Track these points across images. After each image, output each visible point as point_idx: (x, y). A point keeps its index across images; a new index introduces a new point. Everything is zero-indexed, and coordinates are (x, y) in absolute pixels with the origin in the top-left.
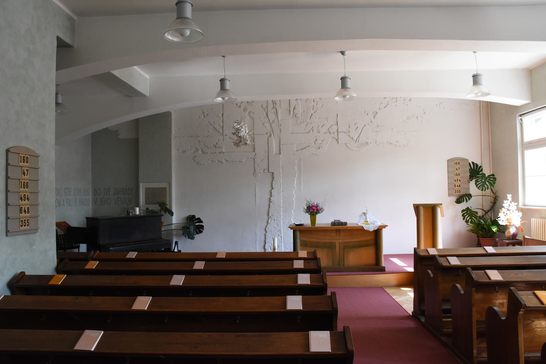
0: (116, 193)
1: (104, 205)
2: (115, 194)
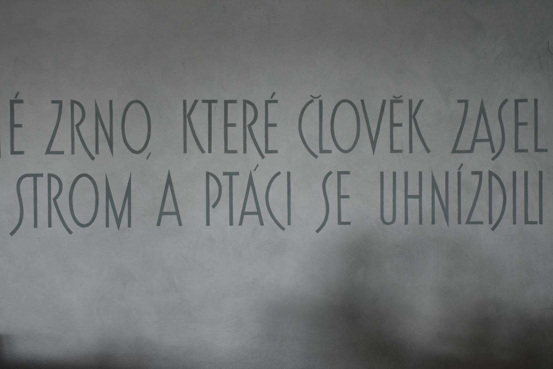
0: (475, 140)
1: (196, 102)
2: (465, 144)
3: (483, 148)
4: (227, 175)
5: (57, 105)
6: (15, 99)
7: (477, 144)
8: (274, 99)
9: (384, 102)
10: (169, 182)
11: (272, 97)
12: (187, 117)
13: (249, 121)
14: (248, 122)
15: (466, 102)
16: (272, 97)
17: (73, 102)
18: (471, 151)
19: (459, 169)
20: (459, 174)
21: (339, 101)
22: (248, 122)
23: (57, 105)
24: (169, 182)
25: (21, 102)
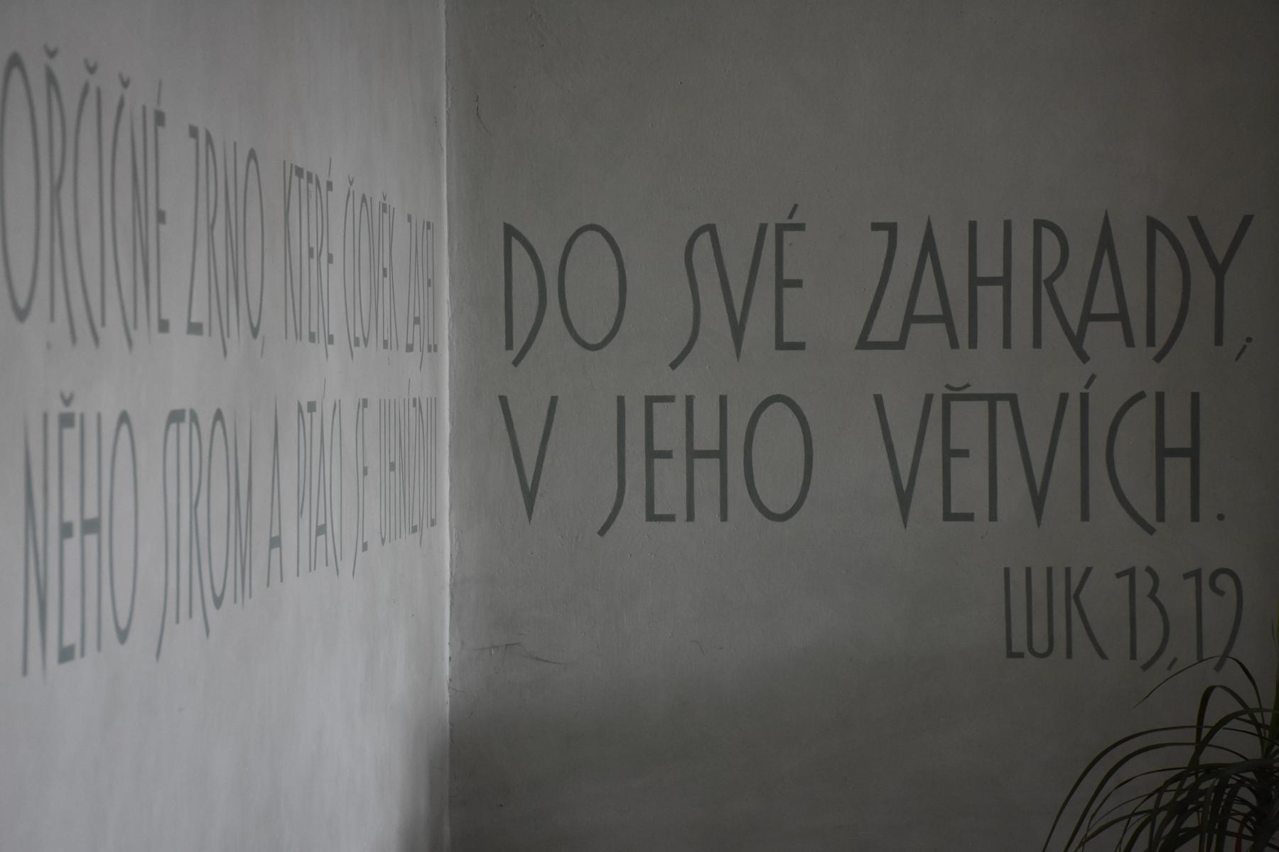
0: (911, 318)
2: (887, 328)
3: (928, 336)
4: (721, 446)
5: (884, 235)
6: (790, 221)
7: (915, 329)
8: (795, 220)
9: (763, 228)
10: (530, 497)
11: (791, 217)
13: (1047, 270)
14: (1046, 272)
15: (891, 228)
16: (791, 217)
17: (1039, 225)
18: (900, 344)
19: (1087, 386)
20: (1084, 398)
21: (578, 227)
22: (1046, 272)
23: (884, 235)
24: (530, 497)
25: (800, 227)
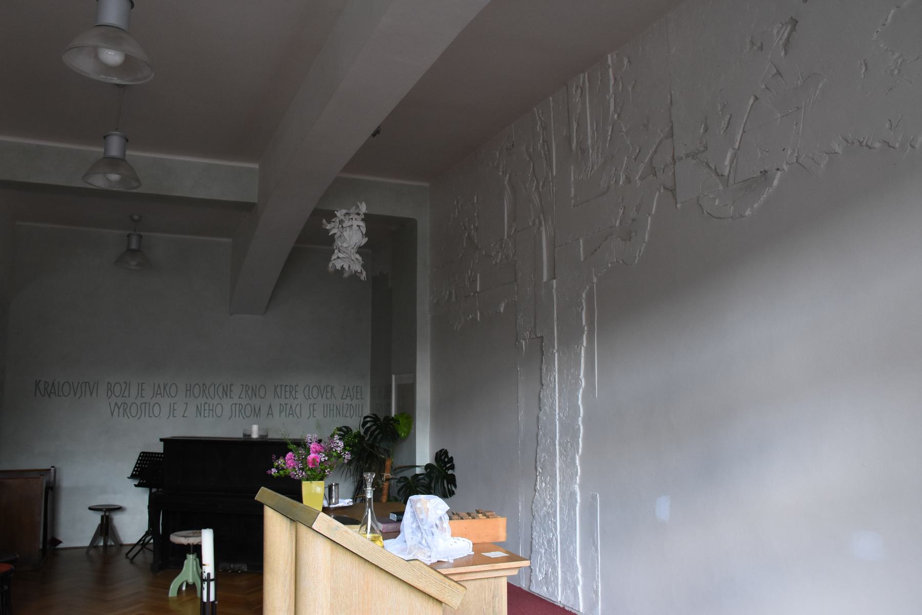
0: (347, 396)
2: (344, 397)
12: (275, 389)
